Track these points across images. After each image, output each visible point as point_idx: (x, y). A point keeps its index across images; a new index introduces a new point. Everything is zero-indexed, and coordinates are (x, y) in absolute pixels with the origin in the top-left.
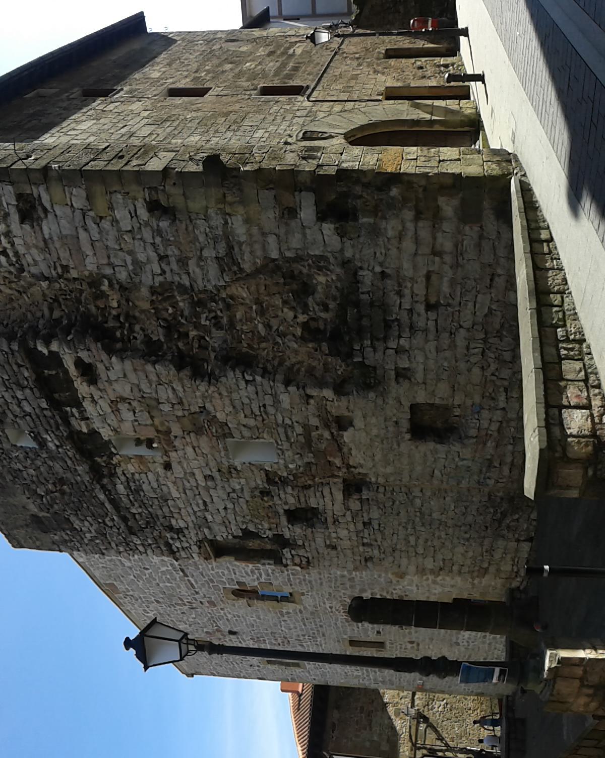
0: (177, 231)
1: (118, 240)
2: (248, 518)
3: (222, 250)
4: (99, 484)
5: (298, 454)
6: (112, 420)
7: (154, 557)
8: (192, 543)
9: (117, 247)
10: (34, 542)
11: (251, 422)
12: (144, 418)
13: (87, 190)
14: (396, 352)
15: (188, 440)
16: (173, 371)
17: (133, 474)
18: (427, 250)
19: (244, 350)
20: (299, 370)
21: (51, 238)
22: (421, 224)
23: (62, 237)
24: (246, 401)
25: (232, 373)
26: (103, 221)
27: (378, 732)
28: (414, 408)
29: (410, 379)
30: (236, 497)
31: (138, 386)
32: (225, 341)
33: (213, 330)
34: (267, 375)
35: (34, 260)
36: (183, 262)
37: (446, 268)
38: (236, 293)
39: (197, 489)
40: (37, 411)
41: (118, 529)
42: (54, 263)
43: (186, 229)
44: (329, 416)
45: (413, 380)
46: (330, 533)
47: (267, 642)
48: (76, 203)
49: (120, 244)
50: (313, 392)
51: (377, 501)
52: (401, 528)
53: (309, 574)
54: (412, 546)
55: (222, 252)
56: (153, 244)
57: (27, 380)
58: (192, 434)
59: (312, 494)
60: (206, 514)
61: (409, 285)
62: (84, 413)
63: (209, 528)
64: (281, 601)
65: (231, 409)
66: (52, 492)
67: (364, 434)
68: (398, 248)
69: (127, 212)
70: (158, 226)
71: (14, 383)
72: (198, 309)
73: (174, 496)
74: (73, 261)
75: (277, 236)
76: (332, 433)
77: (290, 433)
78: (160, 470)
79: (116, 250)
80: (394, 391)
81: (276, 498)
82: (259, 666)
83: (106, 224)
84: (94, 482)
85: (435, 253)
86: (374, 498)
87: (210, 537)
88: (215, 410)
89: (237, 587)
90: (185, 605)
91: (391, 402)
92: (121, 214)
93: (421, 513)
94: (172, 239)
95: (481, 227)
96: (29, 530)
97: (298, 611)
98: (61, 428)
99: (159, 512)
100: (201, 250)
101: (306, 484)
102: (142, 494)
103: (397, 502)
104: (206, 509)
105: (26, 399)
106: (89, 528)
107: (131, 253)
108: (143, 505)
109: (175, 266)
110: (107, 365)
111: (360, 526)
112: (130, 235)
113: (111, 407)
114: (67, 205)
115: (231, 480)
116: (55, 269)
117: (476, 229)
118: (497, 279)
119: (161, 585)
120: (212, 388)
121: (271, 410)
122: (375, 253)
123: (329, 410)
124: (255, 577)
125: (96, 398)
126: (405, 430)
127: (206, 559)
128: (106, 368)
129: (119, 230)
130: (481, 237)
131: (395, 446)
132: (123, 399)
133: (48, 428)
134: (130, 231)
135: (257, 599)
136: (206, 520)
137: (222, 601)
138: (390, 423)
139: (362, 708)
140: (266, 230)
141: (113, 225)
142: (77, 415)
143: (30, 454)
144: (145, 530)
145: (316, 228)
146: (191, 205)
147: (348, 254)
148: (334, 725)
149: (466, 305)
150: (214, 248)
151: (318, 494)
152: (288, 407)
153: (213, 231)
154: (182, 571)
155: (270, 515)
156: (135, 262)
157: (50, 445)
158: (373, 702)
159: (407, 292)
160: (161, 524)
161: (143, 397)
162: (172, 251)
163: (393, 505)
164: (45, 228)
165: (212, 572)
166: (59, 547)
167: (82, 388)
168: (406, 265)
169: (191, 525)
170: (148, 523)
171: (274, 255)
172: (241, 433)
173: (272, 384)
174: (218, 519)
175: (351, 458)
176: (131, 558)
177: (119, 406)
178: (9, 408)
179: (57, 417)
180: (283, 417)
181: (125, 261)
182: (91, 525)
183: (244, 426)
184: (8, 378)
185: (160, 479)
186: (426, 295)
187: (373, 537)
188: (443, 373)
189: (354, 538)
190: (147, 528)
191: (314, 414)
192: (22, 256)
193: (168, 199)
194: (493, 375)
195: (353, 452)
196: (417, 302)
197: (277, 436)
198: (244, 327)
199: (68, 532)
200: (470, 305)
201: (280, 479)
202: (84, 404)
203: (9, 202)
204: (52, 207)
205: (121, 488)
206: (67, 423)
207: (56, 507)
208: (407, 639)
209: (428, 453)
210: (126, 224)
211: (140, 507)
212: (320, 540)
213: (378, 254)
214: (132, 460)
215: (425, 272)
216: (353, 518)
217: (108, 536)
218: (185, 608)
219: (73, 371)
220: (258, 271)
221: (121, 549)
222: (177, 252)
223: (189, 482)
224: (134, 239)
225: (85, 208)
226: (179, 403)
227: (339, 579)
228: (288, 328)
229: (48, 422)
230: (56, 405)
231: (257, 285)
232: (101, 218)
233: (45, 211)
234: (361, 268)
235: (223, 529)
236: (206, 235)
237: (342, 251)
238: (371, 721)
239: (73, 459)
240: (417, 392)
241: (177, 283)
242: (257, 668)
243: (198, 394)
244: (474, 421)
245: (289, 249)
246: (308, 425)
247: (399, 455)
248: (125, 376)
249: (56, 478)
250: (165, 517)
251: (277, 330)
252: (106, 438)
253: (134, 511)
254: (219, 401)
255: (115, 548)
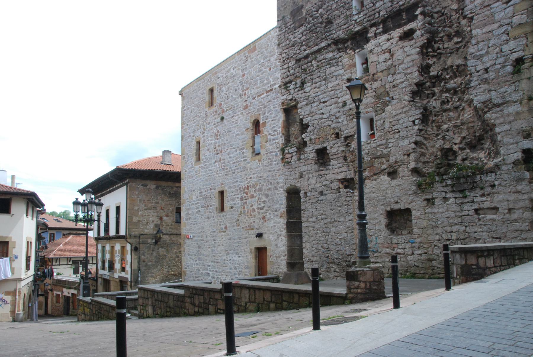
0: (506, 76)
1: (495, 45)
2: (317, 127)
5: (369, 152)
6: (378, 50)
7: (280, 74)
9: (490, 45)
10: (282, 6)
11: (387, 125)
12: (382, 66)
13: (526, 23)
14: (443, 198)
17: (341, 61)
18: (511, 207)
19: (431, 118)
20: (422, 148)
21: (491, 9)
23: (493, 14)
25: (419, 113)
26: (506, 35)
27: (144, 214)
28: (408, 211)
31: (402, 63)
32: (434, 107)
33: (440, 101)
34: (418, 132)
38: (466, 111)
40: (378, 10)
41: (299, 53)
43: (507, 81)
44: (397, 167)
46: (312, 173)
48: (516, 19)
49: (492, 46)
50: (412, 157)
52: (321, 212)
54: (308, 220)
55: (496, 102)
56: (495, 64)
57: (397, 4)
58: (374, 93)
59: (340, 161)
60: (318, 103)
61: (489, 199)
63: (307, 105)
65: (394, 114)
66: (322, 17)
67: (387, 186)
70: (507, 66)
72: (452, 91)
76: (385, 169)
77: (382, 147)
78: (346, 77)
80: (418, 199)
82: (194, 136)
83: (504, 37)
84: (332, 41)
87: (300, 105)
89: (261, 122)
90: (243, 91)
91: (410, 198)
93: (333, 222)
94: (500, 74)
96: (291, 4)
97: (245, 158)
98: (369, 23)
99: (315, 76)
100: (495, 90)
101: (347, 158)
102: (328, 67)
103: (340, 208)
104: (321, 102)
105: (384, 3)
106: (298, 36)
107: (487, 53)
110: (414, 46)
112: (499, 51)
113: (386, 49)
114: (514, 14)
115: (345, 116)
116: (471, 13)
117: (527, 228)
119: (258, 77)
120: (407, 103)
121: (397, 136)
122: (506, 181)
124: (271, 132)
125: (390, 41)
126: (392, 207)
127: (283, 103)
128: (412, 45)
129: (501, 45)
132: (392, 56)
134: (501, 51)
135: (252, 134)
139: (158, 203)
141: (504, 41)
142: (378, 31)
143: (348, 5)
146: (525, 81)
147: (503, 167)
148: (146, 186)
149: (480, 228)
151: (341, 165)
153: (508, 96)
154: (271, 90)
155: (321, 139)
156: (482, 56)
158: (163, 210)
159: (484, 199)
160: (306, 78)
161: (395, 66)
162: (491, 75)
164: (497, 4)
165: (272, 107)
166: (281, 20)
167: (397, 33)
168: (501, 197)
169: (308, 94)
170: (305, 70)
171: (497, 130)
172: (379, 120)
173: (415, 135)
175: (370, 181)
176: (278, 60)
181: (481, 50)
182: (300, 38)
183: (384, 122)
186: (483, 209)
187: (312, 197)
190: (302, 69)
191: (397, 159)
193: (527, 69)
197: (379, 140)
198: (445, 117)
199: (293, 26)
200: (481, 230)
201: (349, 143)
202: (386, 34)
205: (330, 55)
206: (372, 26)
207: (311, 19)
208: (228, 225)
210: (505, 48)
212: (306, 168)
214: (351, 61)
215: (498, 206)
216: (325, 185)
217: (292, 48)
218: (240, 92)
219: (407, 28)
220: (483, 121)
222: (492, 77)
224: (497, 53)
225: (513, 24)
226: (394, 86)
227: (276, 181)
228: (448, 141)
230: (384, 21)
231: (473, 122)
232: (508, 34)
234: (496, 175)
235: (307, 113)
236: (505, 92)
238: (151, 209)
239: (347, 29)
241: (471, 79)
242: (192, 135)
243: (402, 95)
245: (502, 137)
246: (389, 156)
248: (408, 56)
250: (312, 79)
251: (447, 135)
252: (365, 47)
253: (314, 62)
254: (398, 107)
255: (284, 52)
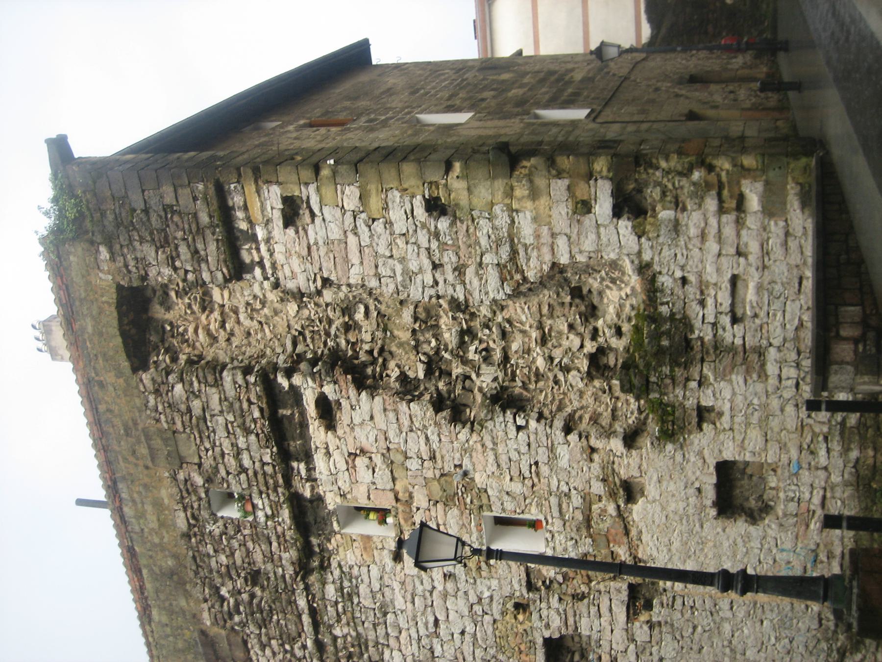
3: (505, 252)
4: (304, 583)
12: (383, 477)
15: (433, 513)
16: (430, 412)
17: (351, 567)
18: (732, 251)
21: (316, 243)
23: (328, 243)
24: (514, 456)
29: (714, 424)
36: (460, 270)
37: (753, 270)
40: (257, 465)
42: (315, 275)
43: (467, 231)
45: (718, 424)
51: (672, 625)
57: (256, 423)
59: (584, 610)
61: (713, 293)
62: (313, 472)
65: (494, 468)
68: (700, 249)
70: (436, 227)
71: (238, 426)
75: (569, 238)
76: (618, 507)
77: (564, 506)
81: (535, 616)
83: (378, 226)
85: (739, 253)
86: (669, 620)
88: (474, 469)
91: (692, 459)
92: (396, 215)
94: (450, 242)
95: (786, 221)
98: (280, 490)
99: (371, 635)
102: (356, 601)
103: (699, 628)
105: (248, 449)
107: (402, 260)
109: (450, 277)
110: (354, 403)
112: (403, 238)
113: (347, 463)
114: (337, 206)
115: (478, 581)
116: (315, 281)
118: (804, 282)
122: (676, 255)
123: (617, 470)
128: (352, 407)
130: (787, 234)
131: (698, 527)
133: (264, 489)
136: (433, 653)
140: (556, 230)
141: (385, 227)
147: (647, 257)
149: (775, 315)
151: (593, 610)
152: (566, 465)
155: (523, 647)
156: (406, 272)
159: (710, 302)
162: (449, 259)
163: (693, 633)
164: (311, 232)
167: (317, 433)
168: (709, 269)
171: (564, 260)
172: (502, 504)
173: (549, 431)
177: (358, 461)
178: (223, 463)
180: (559, 481)
183: (507, 493)
184: (233, 419)
185: (386, 577)
188: (752, 414)
195: (644, 538)
196: (721, 313)
197: (548, 510)
200: (779, 315)
204: (321, 209)
205: (331, 591)
209: (739, 540)
213: (679, 256)
215: (729, 276)
219: (311, 410)
222: (454, 259)
223: (422, 583)
229: (266, 483)
234: (660, 273)
236: (489, 237)
237: (639, 253)
240: (723, 443)
243: (456, 444)
244: (793, 488)
245: (581, 252)
247: (703, 543)
248: (372, 418)
249: (251, 570)
254: (480, 456)
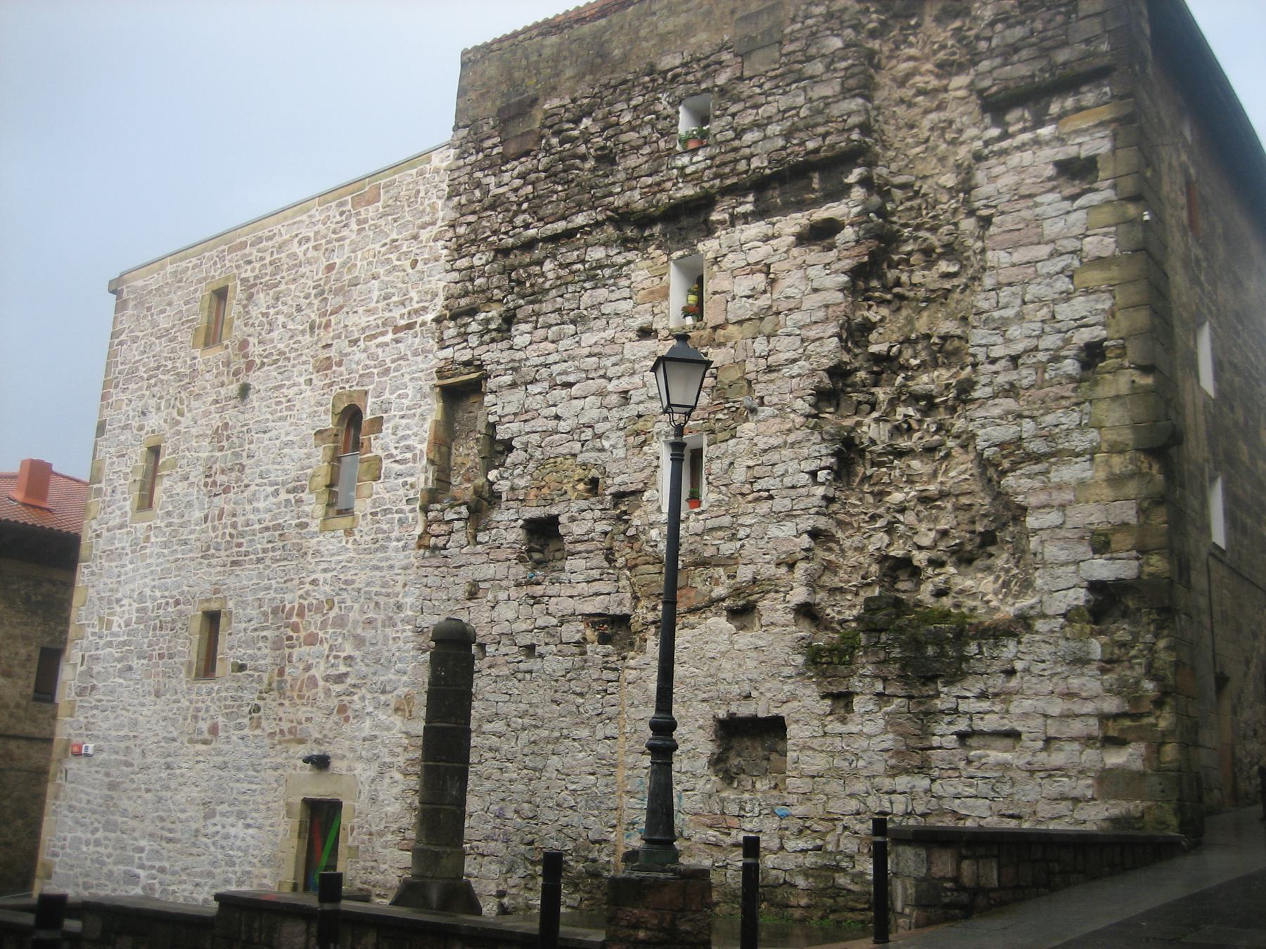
2: (538, 454)
8: (477, 352)
16: (827, 363)
17: (628, 276)
21: (1036, 205)
22: (1094, 722)
23: (1038, 220)
24: (779, 470)
26: (1067, 280)
30: (583, 438)
35: (996, 177)
36: (1011, 390)
39: (601, 377)
40: (747, 151)
42: (995, 207)
43: (1063, 397)
47: (219, 454)
51: (583, 668)
53: (404, 548)
59: (594, 563)
60: (546, 385)
61: (997, 708)
63: (513, 385)
64: (331, 492)
65: (762, 446)
69: (1084, 314)
70: (1066, 357)
73: (584, 336)
74: (999, 234)
75: (1060, 527)
76: (723, 600)
77: (720, 534)
79: (1023, 295)
81: (583, 504)
83: (1063, 284)
87: (492, 383)
91: (786, 688)
94: (1047, 376)
98: (717, 182)
99: (547, 307)
102: (587, 285)
107: (1020, 317)
108: (562, 283)
109: (1001, 379)
111: (526, 640)
113: (757, 263)
114: (1087, 229)
115: (621, 433)
116: (987, 206)
120: (799, 420)
121: (764, 507)
122: (1043, 661)
124: (395, 452)
126: (733, 709)
131: (702, 696)
133: (717, 161)
135: (336, 449)
136: (531, 383)
137: (331, 385)
138: (747, 687)
140: (1069, 511)
141: (1062, 293)
144: (506, 276)
145: (1075, 581)
147: (1040, 625)
149: (971, 785)
150: (1035, 436)
151: (596, 574)
154: (410, 326)
156: (1005, 322)
157: (685, 160)
159: (985, 705)
162: (1026, 376)
163: (574, 693)
167: (793, 223)
171: (1031, 522)
173: (813, 511)
174: (534, 403)
179: (735, 180)
183: (732, 463)
185: (620, 320)
187: (501, 660)
188: (845, 759)
189: (496, 630)
190: (511, 281)
192: (1002, 160)
194: (845, 828)
197: (714, 514)
200: (972, 791)
203: (1084, 147)
205: (597, 253)
206: (727, 191)
208: (221, 720)
211: (558, 278)
214: (657, 280)
215: (1019, 729)
219: (821, 214)
221: (462, 230)
222: (1025, 383)
224: (1043, 321)
233: (1073, 198)
235: (510, 409)
236: (1056, 426)
237: (1044, 616)
245: (1042, 542)
248: (816, 290)
253: (548, 265)
254: (776, 427)
